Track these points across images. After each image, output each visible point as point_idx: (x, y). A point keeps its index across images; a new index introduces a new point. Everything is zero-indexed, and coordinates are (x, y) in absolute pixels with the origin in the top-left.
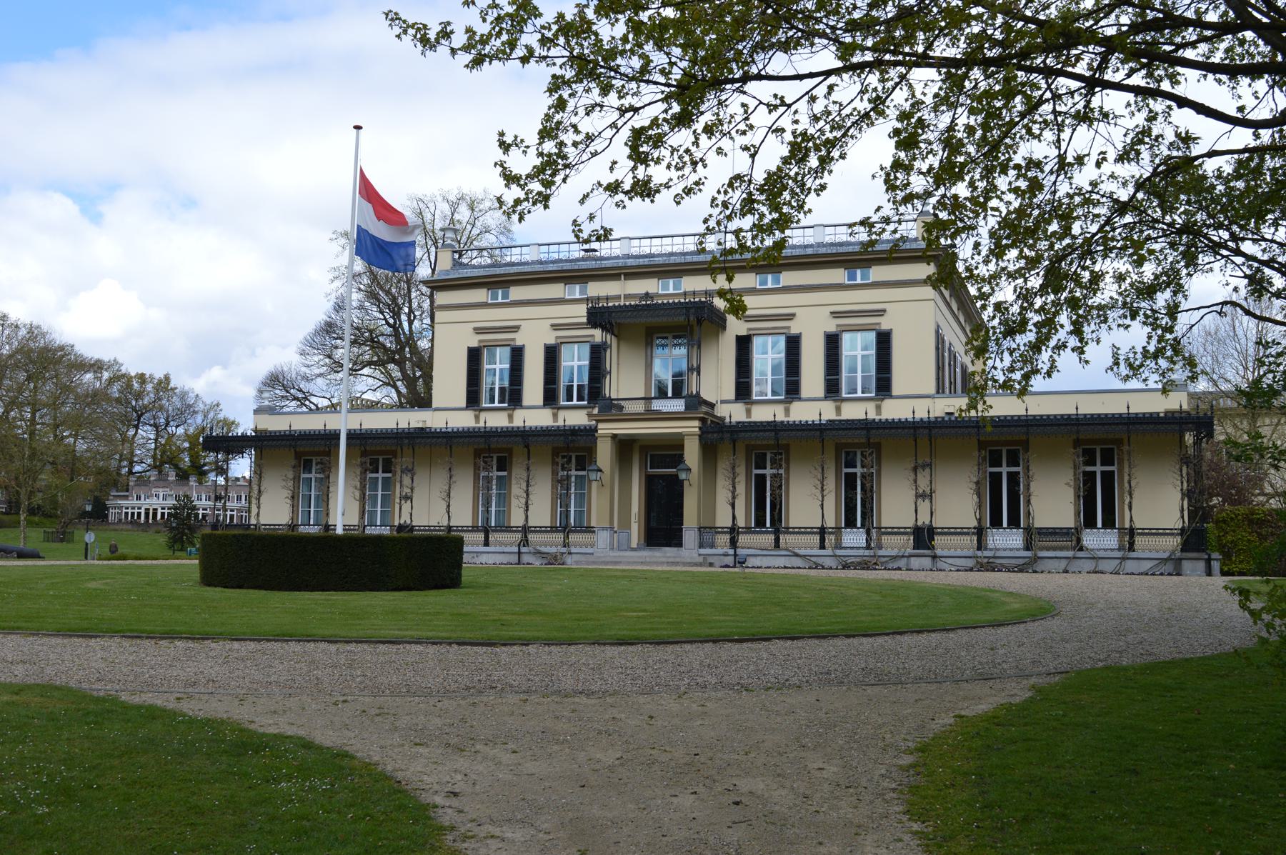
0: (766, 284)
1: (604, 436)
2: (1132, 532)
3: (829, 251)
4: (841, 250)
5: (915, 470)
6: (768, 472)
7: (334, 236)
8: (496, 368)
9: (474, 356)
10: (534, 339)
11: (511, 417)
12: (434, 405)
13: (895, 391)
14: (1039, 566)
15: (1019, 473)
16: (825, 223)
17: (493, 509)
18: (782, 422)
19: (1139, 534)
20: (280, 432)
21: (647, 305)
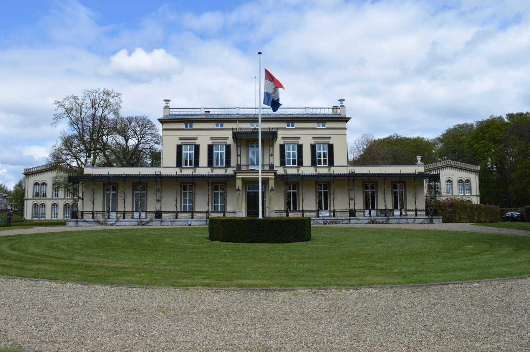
0: (320, 127)
1: (239, 178)
2: (334, 211)
3: (311, 117)
4: (323, 116)
5: (349, 190)
6: (398, 190)
7: (55, 103)
8: (187, 152)
9: (179, 148)
10: (204, 142)
11: (298, 170)
13: (304, 165)
14: (391, 221)
15: (296, 192)
16: (240, 107)
17: (111, 205)
18: (211, 175)
19: (337, 212)
20: (104, 175)
21: (255, 132)
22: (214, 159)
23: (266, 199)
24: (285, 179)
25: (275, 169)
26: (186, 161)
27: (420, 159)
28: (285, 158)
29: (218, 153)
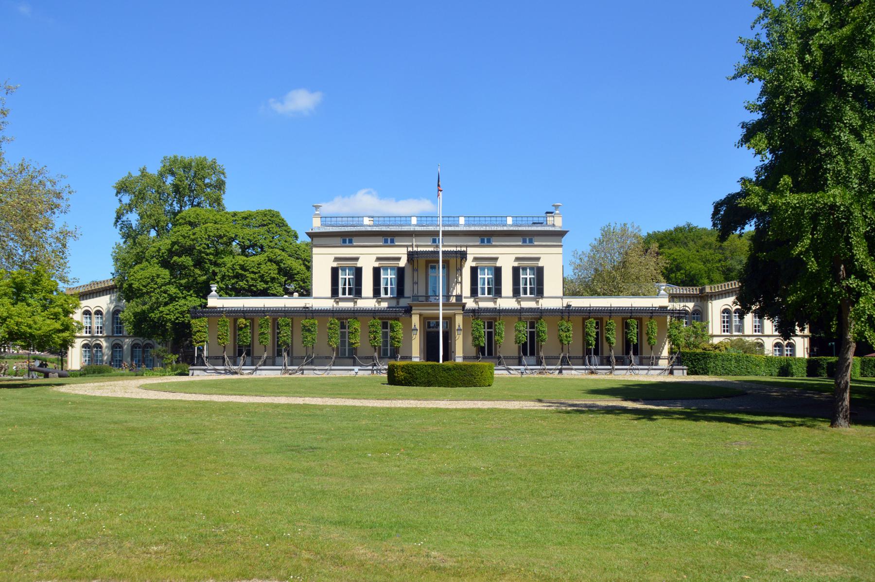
9: (335, 272)
12: (314, 295)
13: (545, 294)
22: (479, 286)
23: (451, 340)
24: (476, 314)
25: (464, 301)
26: (344, 289)
27: (215, 288)
28: (519, 285)
29: (484, 278)
